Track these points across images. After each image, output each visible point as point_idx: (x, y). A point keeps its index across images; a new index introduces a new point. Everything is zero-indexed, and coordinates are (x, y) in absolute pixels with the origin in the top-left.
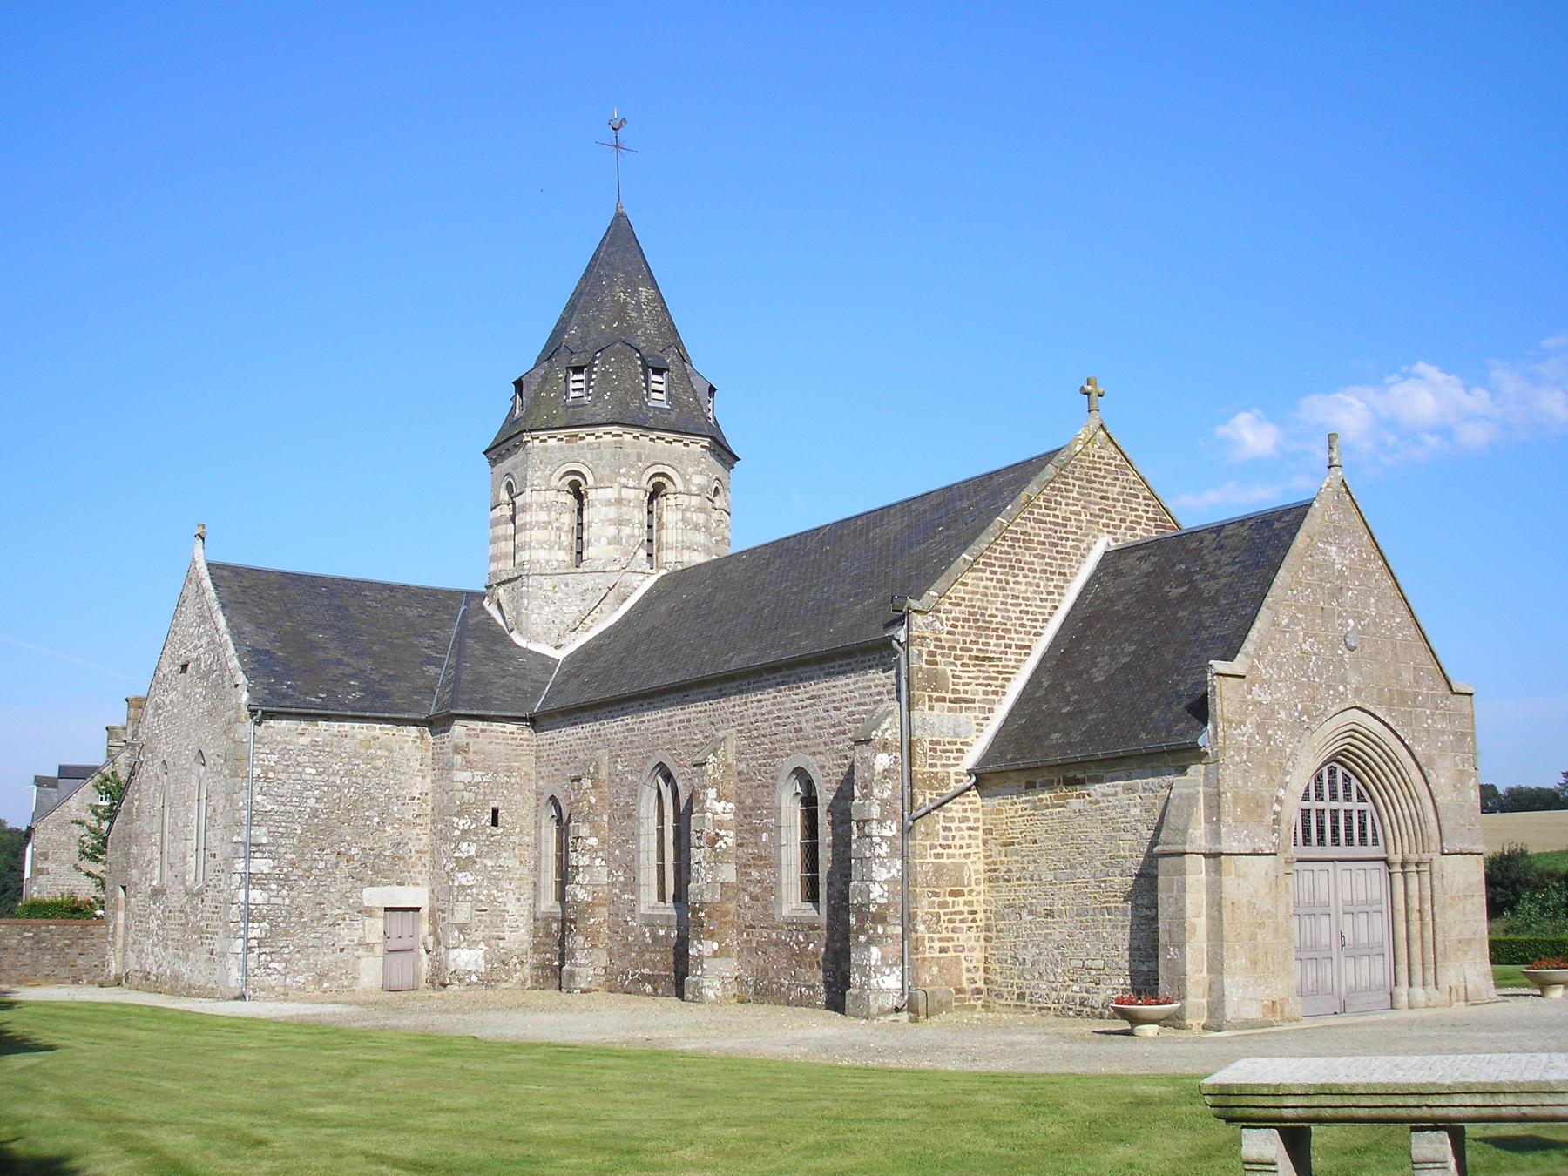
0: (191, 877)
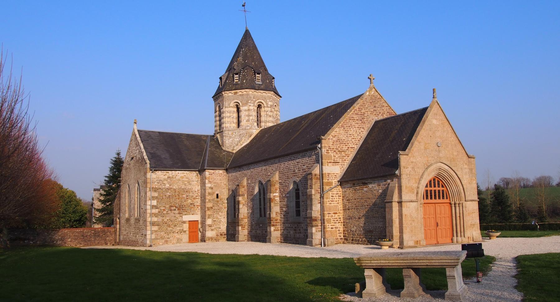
0: (136, 215)
